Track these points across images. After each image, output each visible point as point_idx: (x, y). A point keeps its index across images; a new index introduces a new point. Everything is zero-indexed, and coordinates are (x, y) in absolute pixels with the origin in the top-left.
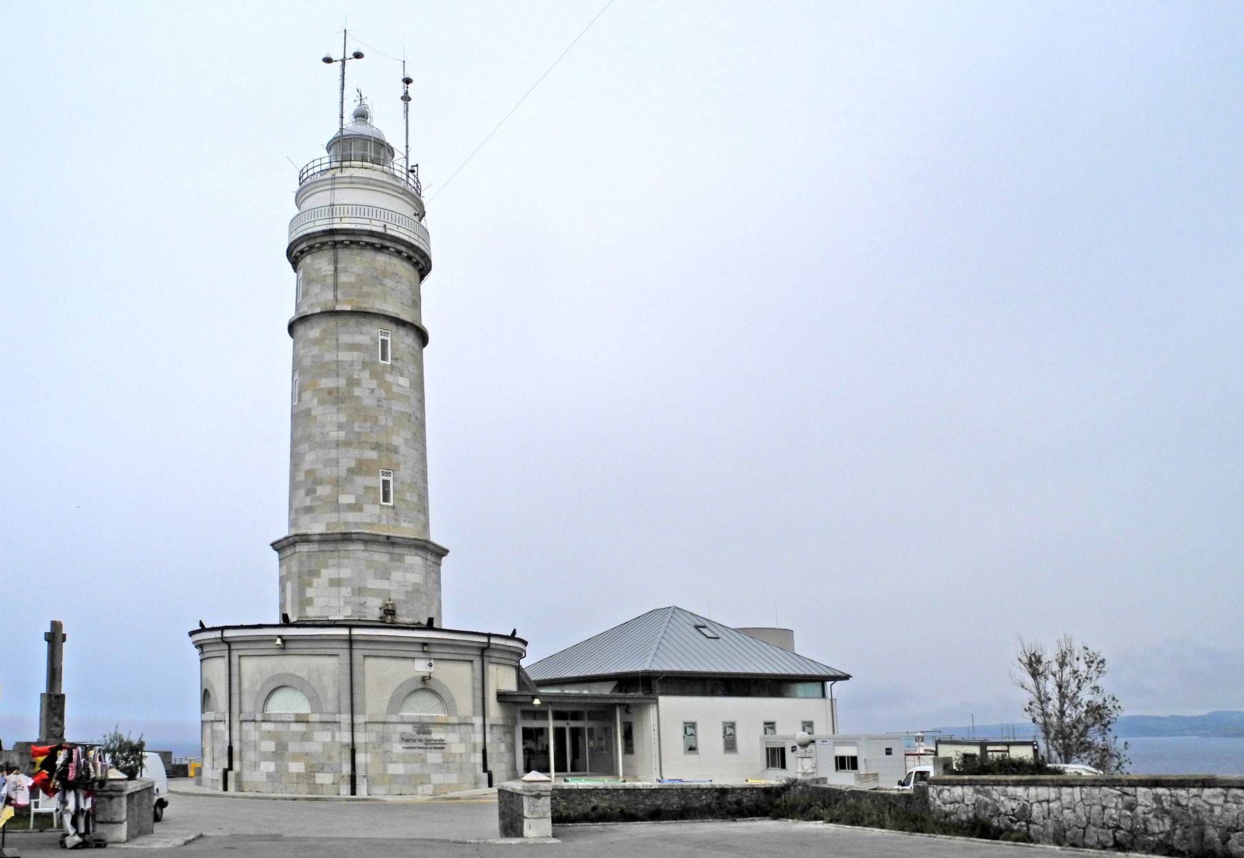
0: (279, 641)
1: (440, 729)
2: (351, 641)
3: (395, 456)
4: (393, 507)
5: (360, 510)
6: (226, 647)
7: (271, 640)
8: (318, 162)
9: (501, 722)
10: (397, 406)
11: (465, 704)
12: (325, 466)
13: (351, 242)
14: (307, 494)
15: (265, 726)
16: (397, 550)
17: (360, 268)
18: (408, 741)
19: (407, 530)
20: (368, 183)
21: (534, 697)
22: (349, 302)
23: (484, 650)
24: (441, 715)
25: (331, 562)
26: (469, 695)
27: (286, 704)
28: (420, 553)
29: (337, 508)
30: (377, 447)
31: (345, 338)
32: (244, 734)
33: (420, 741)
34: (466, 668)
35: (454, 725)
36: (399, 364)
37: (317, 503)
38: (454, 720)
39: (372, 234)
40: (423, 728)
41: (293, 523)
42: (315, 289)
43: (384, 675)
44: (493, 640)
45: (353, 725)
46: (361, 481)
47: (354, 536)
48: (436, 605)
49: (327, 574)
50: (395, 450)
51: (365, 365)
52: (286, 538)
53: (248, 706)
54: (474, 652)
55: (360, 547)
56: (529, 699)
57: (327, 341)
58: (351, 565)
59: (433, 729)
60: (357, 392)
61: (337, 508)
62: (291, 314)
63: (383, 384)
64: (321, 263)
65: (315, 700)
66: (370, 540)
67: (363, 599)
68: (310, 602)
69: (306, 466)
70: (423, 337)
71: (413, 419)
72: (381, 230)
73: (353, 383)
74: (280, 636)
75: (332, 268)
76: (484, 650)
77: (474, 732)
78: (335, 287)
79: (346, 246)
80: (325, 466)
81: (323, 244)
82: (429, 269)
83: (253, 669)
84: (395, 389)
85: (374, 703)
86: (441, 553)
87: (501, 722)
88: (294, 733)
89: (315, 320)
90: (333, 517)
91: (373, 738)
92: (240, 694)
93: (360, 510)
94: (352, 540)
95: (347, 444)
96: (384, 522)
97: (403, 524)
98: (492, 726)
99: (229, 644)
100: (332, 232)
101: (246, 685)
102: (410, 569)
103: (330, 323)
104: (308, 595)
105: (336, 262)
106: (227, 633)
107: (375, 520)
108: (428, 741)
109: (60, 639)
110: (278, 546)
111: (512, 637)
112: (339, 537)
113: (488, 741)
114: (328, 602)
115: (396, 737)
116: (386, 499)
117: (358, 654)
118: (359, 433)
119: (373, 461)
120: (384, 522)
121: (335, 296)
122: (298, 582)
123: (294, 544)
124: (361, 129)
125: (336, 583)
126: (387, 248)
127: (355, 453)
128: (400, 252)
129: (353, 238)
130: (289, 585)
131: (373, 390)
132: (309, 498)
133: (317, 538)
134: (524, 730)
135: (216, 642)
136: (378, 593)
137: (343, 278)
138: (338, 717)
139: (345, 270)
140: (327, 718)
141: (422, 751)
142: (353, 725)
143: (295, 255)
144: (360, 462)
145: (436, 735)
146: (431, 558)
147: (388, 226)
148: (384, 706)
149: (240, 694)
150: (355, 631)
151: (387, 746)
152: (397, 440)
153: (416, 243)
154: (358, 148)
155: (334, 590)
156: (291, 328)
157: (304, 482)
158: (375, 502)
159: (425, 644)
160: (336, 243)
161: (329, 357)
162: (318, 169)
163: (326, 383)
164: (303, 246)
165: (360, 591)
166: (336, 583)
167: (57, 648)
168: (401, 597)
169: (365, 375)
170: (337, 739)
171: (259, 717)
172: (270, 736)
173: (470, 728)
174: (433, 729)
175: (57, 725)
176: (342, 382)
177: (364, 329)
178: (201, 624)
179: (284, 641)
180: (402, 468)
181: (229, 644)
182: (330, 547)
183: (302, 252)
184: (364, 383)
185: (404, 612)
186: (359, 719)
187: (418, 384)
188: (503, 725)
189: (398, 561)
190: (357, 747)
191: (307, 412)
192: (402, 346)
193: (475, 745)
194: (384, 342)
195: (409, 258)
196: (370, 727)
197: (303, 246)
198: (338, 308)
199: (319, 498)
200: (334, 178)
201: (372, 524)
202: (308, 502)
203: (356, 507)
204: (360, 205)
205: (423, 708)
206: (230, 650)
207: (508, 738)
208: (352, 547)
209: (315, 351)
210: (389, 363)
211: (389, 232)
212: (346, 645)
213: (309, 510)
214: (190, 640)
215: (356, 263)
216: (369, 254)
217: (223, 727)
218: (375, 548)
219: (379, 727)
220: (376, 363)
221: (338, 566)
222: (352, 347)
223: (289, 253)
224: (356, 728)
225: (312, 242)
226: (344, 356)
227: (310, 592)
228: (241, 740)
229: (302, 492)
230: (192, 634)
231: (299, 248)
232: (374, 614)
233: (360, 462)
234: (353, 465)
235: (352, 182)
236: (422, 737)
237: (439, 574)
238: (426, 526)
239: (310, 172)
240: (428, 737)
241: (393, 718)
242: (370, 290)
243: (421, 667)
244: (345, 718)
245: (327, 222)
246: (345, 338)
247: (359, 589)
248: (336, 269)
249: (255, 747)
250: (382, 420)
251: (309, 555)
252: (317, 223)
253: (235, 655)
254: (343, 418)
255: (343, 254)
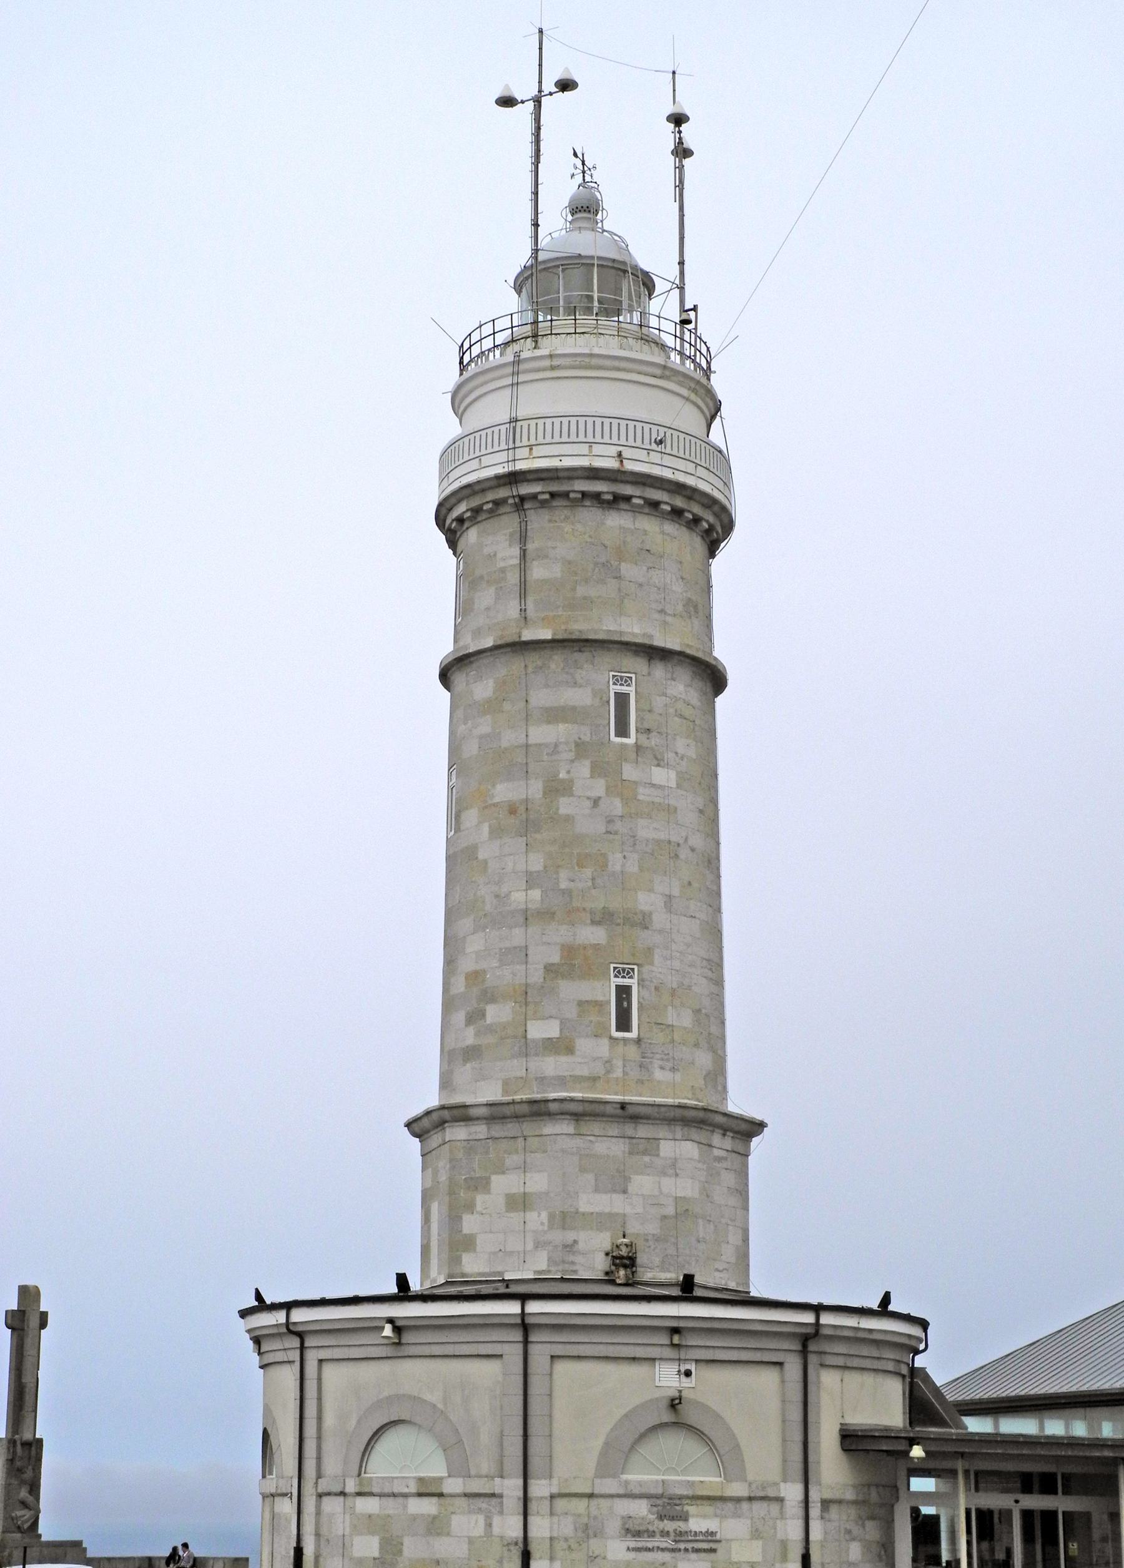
0: (388, 1331)
1: (708, 1509)
2: (525, 1326)
3: (645, 934)
4: (638, 1041)
5: (570, 1050)
6: (295, 1342)
7: (372, 1327)
8: (487, 330)
9: (850, 1495)
10: (647, 830)
11: (764, 1455)
12: (502, 963)
13: (553, 495)
14: (470, 1020)
15: (368, 1506)
16: (643, 1131)
17: (585, 539)
18: (638, 1534)
19: (667, 1088)
20: (588, 365)
21: (912, 1442)
22: (545, 621)
23: (807, 1341)
24: (709, 1480)
25: (513, 1160)
26: (775, 1439)
27: (404, 1458)
28: (695, 1134)
29: (526, 1048)
30: (604, 918)
31: (541, 698)
32: (324, 1519)
33: (665, 1534)
34: (768, 1379)
35: (738, 1500)
36: (654, 741)
37: (490, 1039)
38: (737, 1489)
39: (593, 474)
40: (670, 1506)
41: (446, 1083)
42: (485, 597)
43: (593, 1396)
44: (826, 1319)
45: (526, 1499)
46: (572, 990)
47: (553, 1107)
48: (734, 1238)
49: (503, 1184)
50: (644, 922)
51: (581, 749)
52: (428, 1113)
53: (332, 1466)
54: (786, 1345)
55: (565, 1127)
56: (901, 1446)
57: (507, 706)
58: (547, 1166)
59: (692, 1509)
60: (565, 806)
61: (526, 1048)
62: (444, 647)
63: (622, 788)
64: (495, 541)
65: (455, 1449)
66: (584, 1113)
67: (570, 1236)
68: (468, 1243)
69: (467, 964)
70: (714, 679)
71: (684, 853)
72: (612, 464)
73: (557, 788)
74: (391, 1321)
75: (516, 551)
76: (810, 1339)
77: (782, 1516)
78: (523, 594)
79: (544, 504)
80: (502, 963)
81: (497, 503)
82: (728, 526)
83: (350, 1386)
84: (644, 794)
85: (572, 1456)
86: (752, 1128)
87: (850, 1495)
88: (414, 1518)
89: (485, 661)
90: (516, 1068)
91: (566, 1527)
92: (319, 1438)
93: (570, 1050)
94: (550, 1114)
95: (546, 915)
96: (618, 1073)
97: (659, 1075)
98: (826, 1504)
99: (301, 1335)
100: (513, 478)
101: (329, 1420)
102: (673, 1168)
103: (511, 667)
104: (466, 1230)
105: (523, 538)
106: (299, 1316)
107: (599, 1069)
108: (680, 1535)
109: (34, 1322)
110: (420, 1127)
111: (884, 1309)
112: (525, 1108)
113: (816, 1534)
114: (506, 1246)
115: (613, 1526)
116: (624, 1023)
117: (540, 1353)
118: (567, 893)
119: (596, 947)
120: (618, 1073)
121: (523, 611)
122: (449, 1201)
123: (441, 1124)
124: (585, 244)
125: (520, 1202)
126: (628, 499)
127: (560, 934)
128: (655, 505)
129: (555, 487)
130: (435, 1207)
131: (596, 802)
132: (471, 1031)
133: (483, 1111)
134: (1087, 1516)
135: (285, 1331)
136: (600, 1221)
137: (538, 572)
138: (498, 1485)
139: (542, 555)
140: (476, 1486)
141: (667, 1557)
142: (526, 1499)
143: (455, 519)
144: (569, 950)
145: (697, 1524)
146: (722, 1143)
147: (627, 453)
148: (591, 1463)
149: (319, 1438)
150: (533, 1307)
151: (595, 1545)
152: (645, 901)
153: (690, 481)
154: (582, 286)
155: (516, 1217)
156: (445, 676)
157: (466, 996)
158: (600, 1032)
159: (675, 1331)
160: (523, 499)
161: (510, 738)
162: (488, 344)
163: (504, 792)
164: (461, 509)
165: (565, 1219)
166: (520, 1202)
167: (28, 1342)
168: (653, 1228)
169: (583, 769)
170: (496, 1530)
171: (351, 1486)
172: (370, 1524)
173: (775, 1508)
174: (692, 1509)
175: (24, 1504)
176: (535, 789)
177: (580, 675)
178: (259, 1296)
179: (398, 1330)
180: (657, 959)
181: (301, 1335)
182: (511, 1128)
183: (460, 520)
184: (577, 789)
185: (657, 1260)
186: (540, 1488)
187: (705, 778)
188: (855, 1502)
189: (645, 1152)
190: (533, 1548)
191: (471, 852)
192: (659, 702)
193: (784, 1544)
194: (622, 700)
195: (677, 513)
196: (561, 1504)
197: (461, 509)
198: (527, 635)
199: (490, 1029)
200: (517, 361)
201: (594, 1079)
202: (469, 1037)
203: (562, 1046)
204: (579, 419)
205: (672, 1465)
206: (302, 1348)
207: (872, 1531)
208: (549, 1128)
209: (485, 726)
210: (631, 741)
211: (629, 466)
212: (518, 1336)
213: (471, 1053)
214: (241, 1325)
215: (566, 539)
216: (590, 515)
217: (287, 1507)
218: (596, 1127)
219: (580, 1505)
220: (605, 743)
221: (524, 1168)
222: (554, 715)
223: (440, 521)
224: (533, 1506)
225: (475, 502)
226: (542, 734)
227: (470, 1224)
228: (318, 1535)
229: (459, 1017)
230: (244, 1314)
231: (455, 513)
232: (593, 1265)
233: (569, 950)
234: (556, 959)
235: (555, 365)
236: (669, 1526)
237: (743, 1174)
238: (717, 1075)
239: (476, 350)
240: (681, 1525)
241: (609, 1486)
242: (593, 592)
243: (668, 1377)
244: (511, 1487)
245: (503, 457)
246: (541, 698)
247: (564, 1214)
248: (524, 553)
249: (344, 1547)
250: (616, 862)
251: (471, 1146)
252: (486, 461)
253: (312, 1357)
254: (536, 863)
255: (538, 520)
